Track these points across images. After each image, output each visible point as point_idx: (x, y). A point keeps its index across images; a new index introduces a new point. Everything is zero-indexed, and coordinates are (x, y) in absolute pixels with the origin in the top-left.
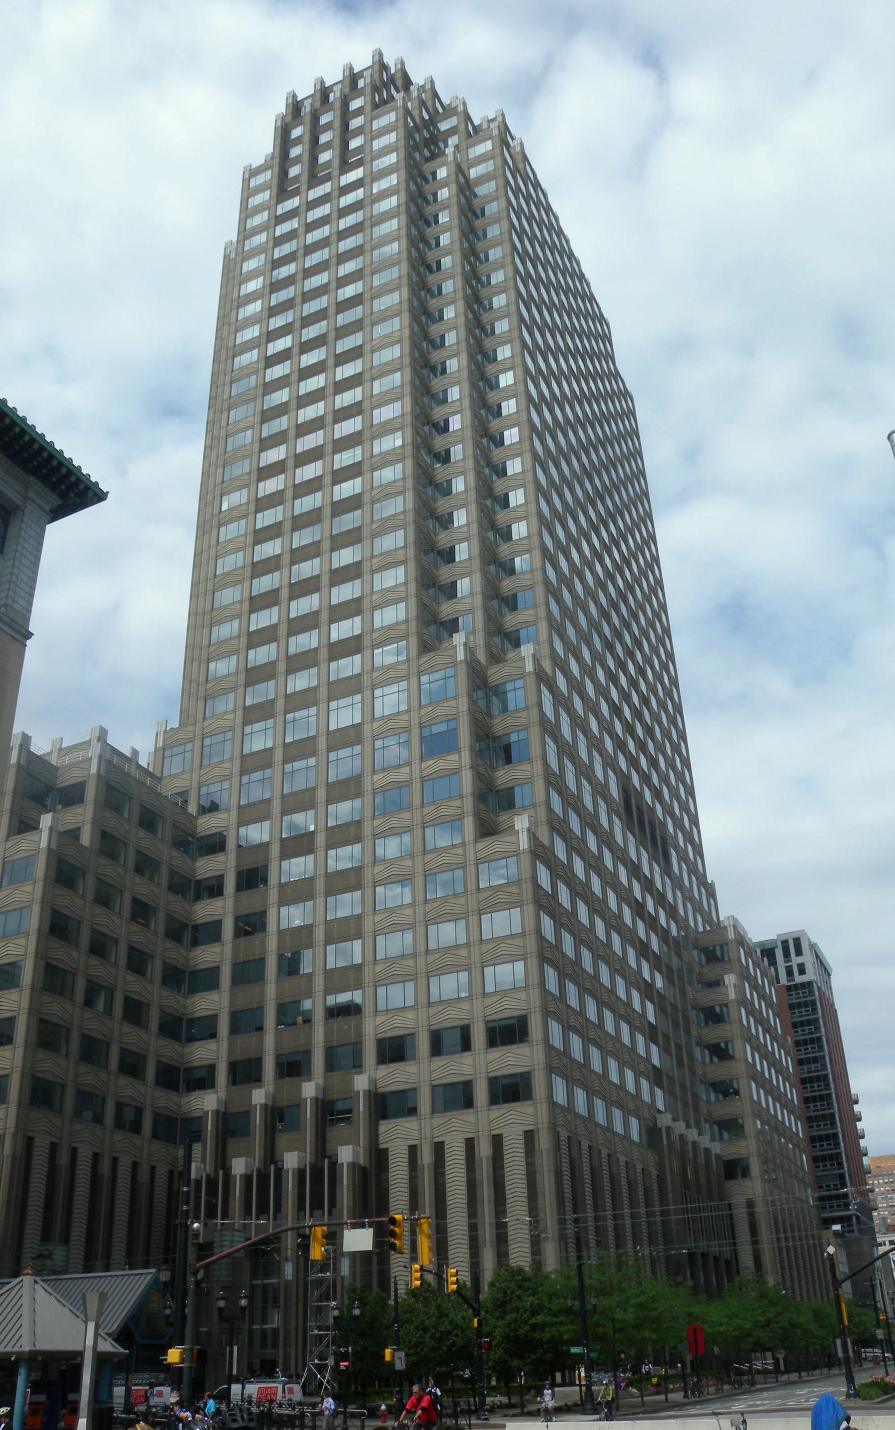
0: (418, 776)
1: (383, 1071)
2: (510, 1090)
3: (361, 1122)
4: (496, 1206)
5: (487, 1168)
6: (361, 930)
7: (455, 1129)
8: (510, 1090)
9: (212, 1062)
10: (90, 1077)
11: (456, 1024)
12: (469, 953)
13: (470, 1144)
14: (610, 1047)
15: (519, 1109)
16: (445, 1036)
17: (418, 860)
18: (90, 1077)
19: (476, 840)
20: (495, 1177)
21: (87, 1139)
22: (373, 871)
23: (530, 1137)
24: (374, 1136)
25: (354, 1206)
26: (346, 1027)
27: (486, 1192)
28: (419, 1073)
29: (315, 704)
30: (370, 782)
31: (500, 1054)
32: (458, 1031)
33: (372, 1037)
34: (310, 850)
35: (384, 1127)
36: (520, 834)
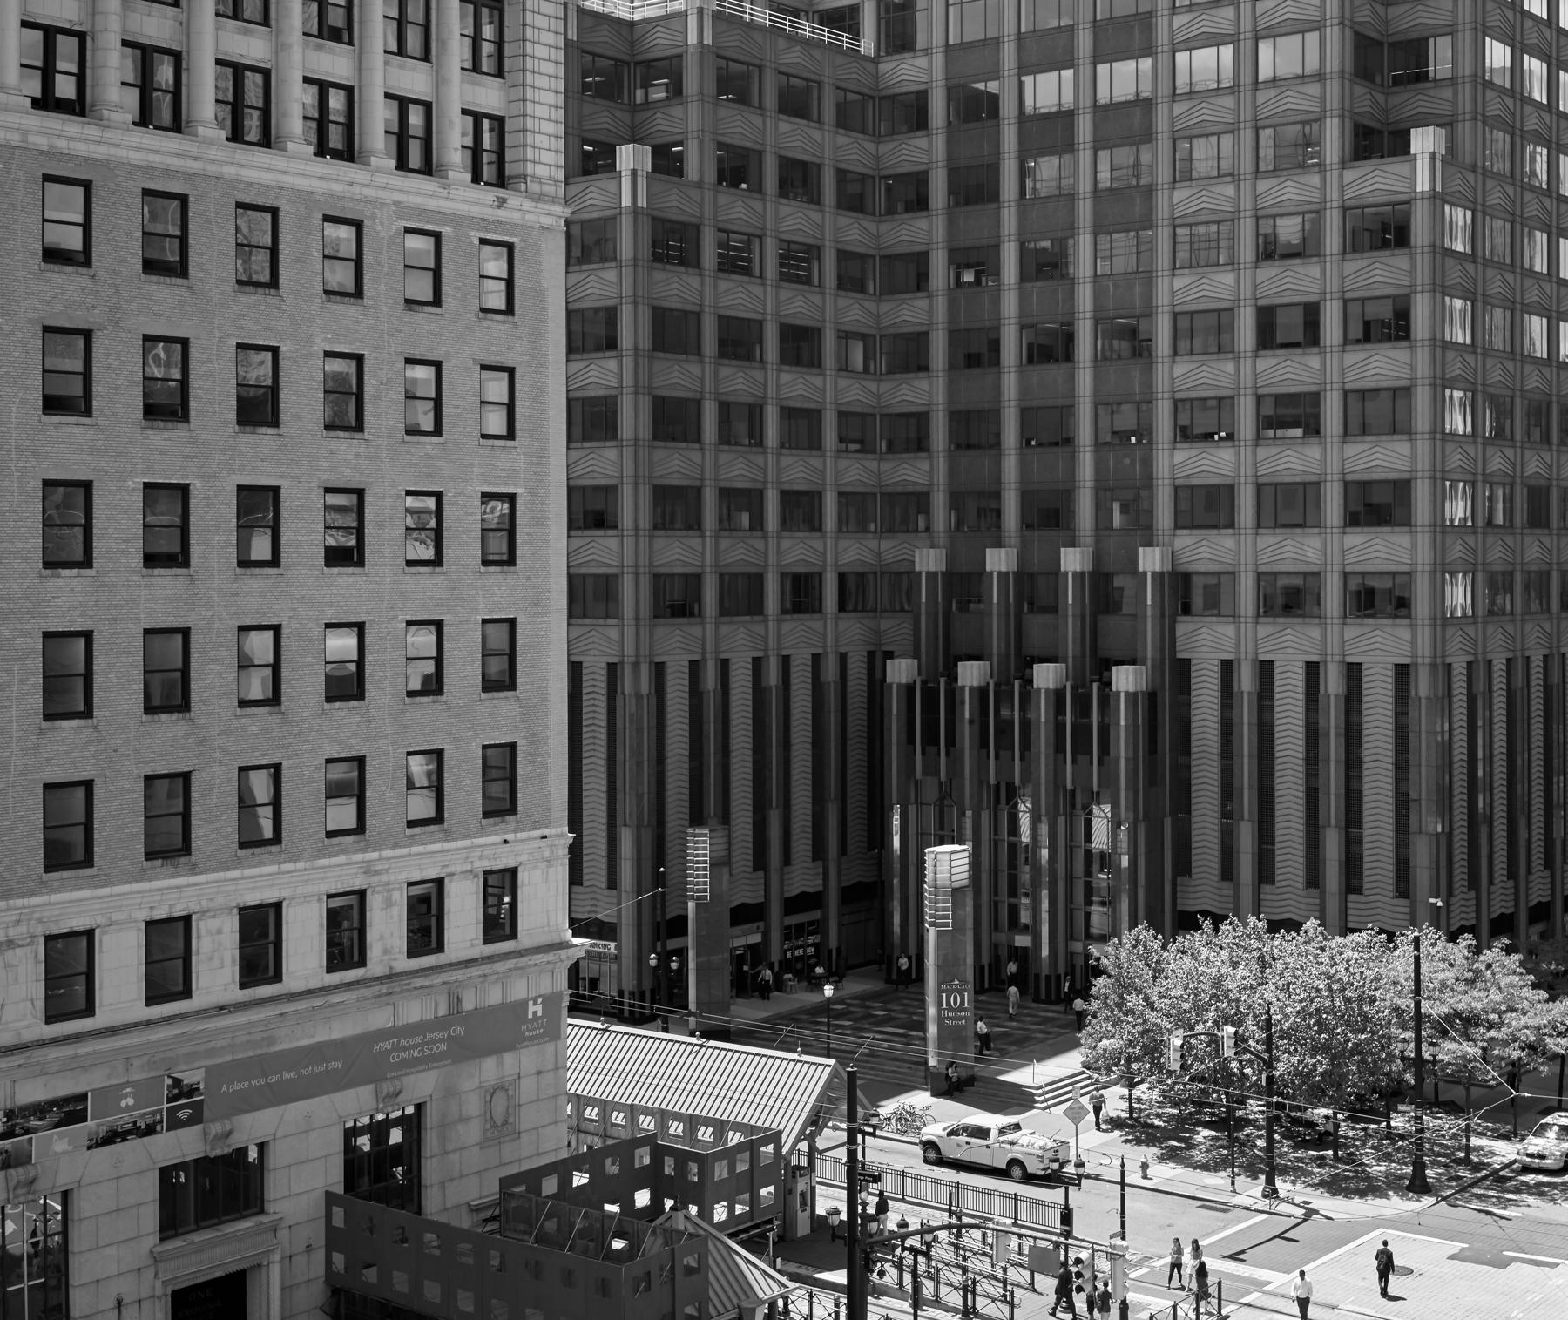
0: (1249, 27)
1: (1185, 541)
2: (1374, 599)
3: (1149, 620)
4: (1347, 768)
5: (1338, 701)
6: (1151, 387)
7: (1290, 646)
8: (1374, 599)
9: (922, 87)
10: (738, 381)
11: (1297, 299)
12: (1323, 364)
13: (1313, 671)
14: (1532, 38)
15: (1389, 630)
16: (1281, 318)
17: (1245, 97)
18: (738, 381)
19: (1343, 164)
20: (1348, 724)
21: (739, 643)
22: (1171, 197)
23: (1403, 674)
24: (1168, 639)
25: (1136, 758)
26: (1127, 461)
27: (1334, 748)
28: (1239, 551)
29: (1070, 62)
30: (1167, 463)
31: (1365, 262)
32: (1300, 311)
33: (1167, 482)
34: (1066, 60)
35: (1184, 626)
36: (1419, 163)
